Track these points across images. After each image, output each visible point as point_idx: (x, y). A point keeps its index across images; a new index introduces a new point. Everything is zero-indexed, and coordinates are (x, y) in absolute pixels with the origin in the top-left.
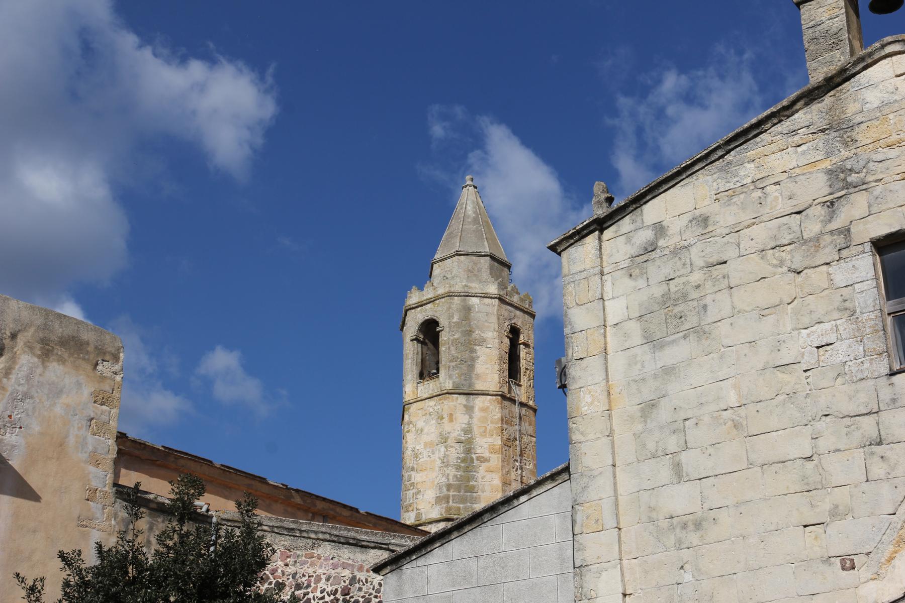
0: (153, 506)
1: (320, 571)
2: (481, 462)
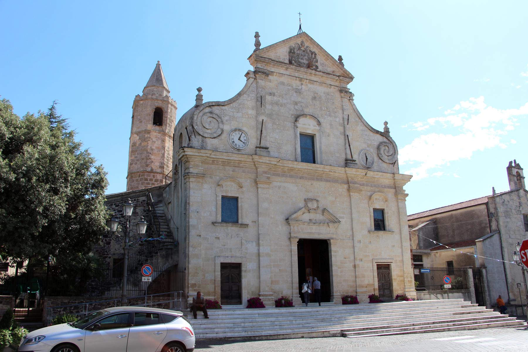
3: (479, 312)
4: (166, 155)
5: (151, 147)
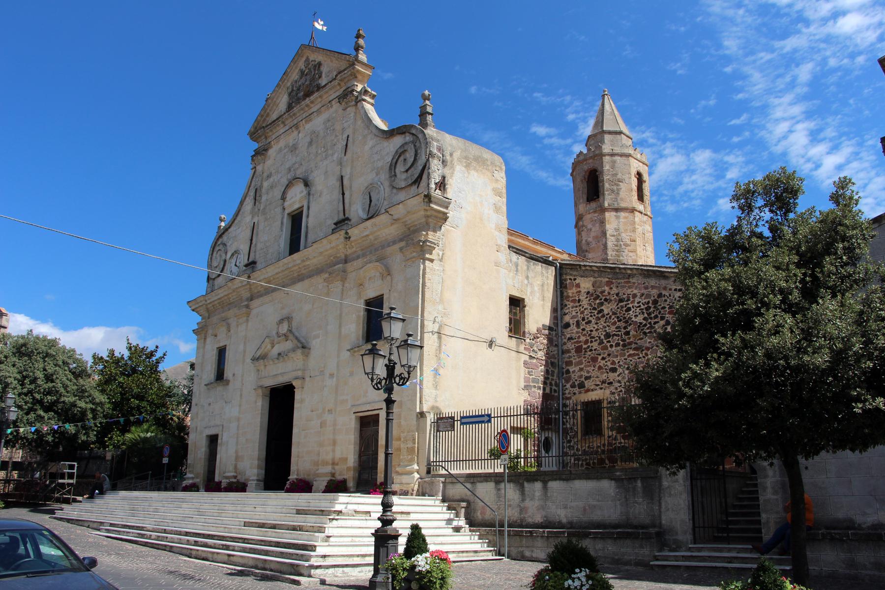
1: (635, 291)
3: (294, 529)
4: (610, 244)
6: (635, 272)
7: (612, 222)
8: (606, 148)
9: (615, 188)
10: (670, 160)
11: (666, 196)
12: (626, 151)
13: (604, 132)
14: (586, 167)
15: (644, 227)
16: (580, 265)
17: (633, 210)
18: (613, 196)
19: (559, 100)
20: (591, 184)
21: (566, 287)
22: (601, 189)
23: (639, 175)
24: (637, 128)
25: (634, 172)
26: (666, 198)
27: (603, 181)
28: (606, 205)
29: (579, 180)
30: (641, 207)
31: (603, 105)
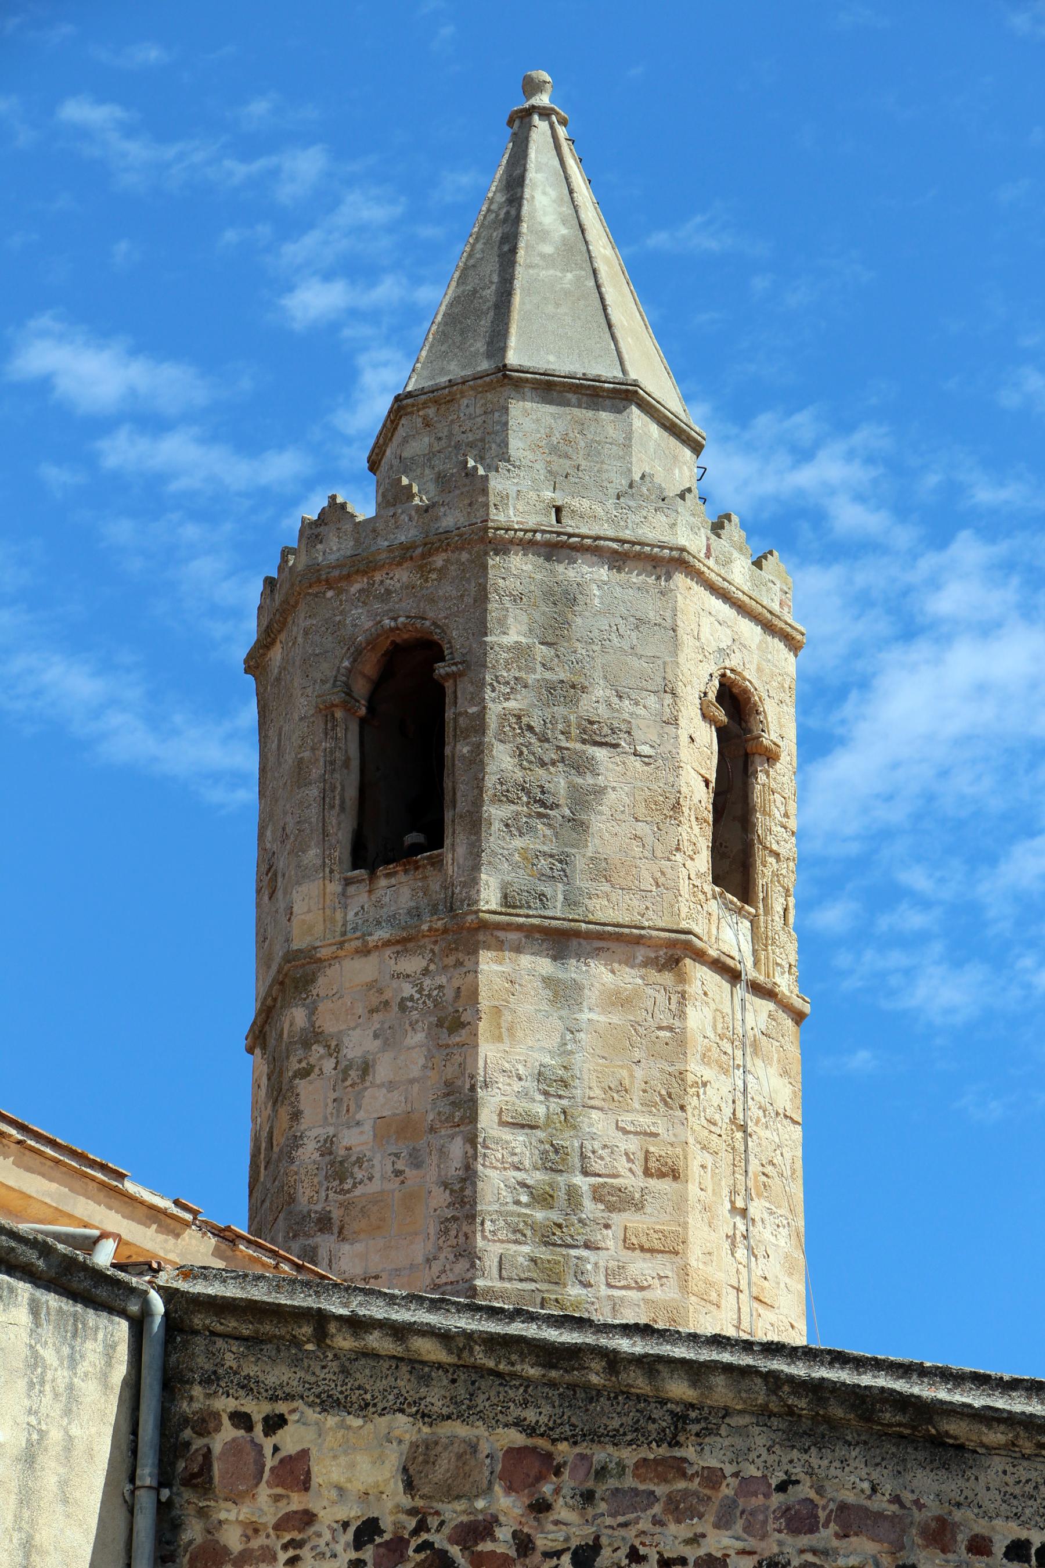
0: (641, 953)
2: (611, 1208)
4: (496, 1185)
5: (327, 1147)
6: (722, 1392)
7: (524, 1026)
8: (518, 499)
9: (559, 782)
10: (966, 662)
11: (924, 903)
12: (653, 529)
13: (506, 380)
14: (362, 620)
15: (744, 1075)
16: (320, 1319)
17: (674, 953)
18: (542, 840)
19: (240, 170)
20: (395, 746)
21: (200, 1479)
22: (458, 782)
23: (734, 707)
24: (765, 423)
25: (697, 679)
26: (915, 920)
27: (479, 724)
28: (489, 897)
29: (303, 704)
30: (728, 935)
31: (515, 184)
